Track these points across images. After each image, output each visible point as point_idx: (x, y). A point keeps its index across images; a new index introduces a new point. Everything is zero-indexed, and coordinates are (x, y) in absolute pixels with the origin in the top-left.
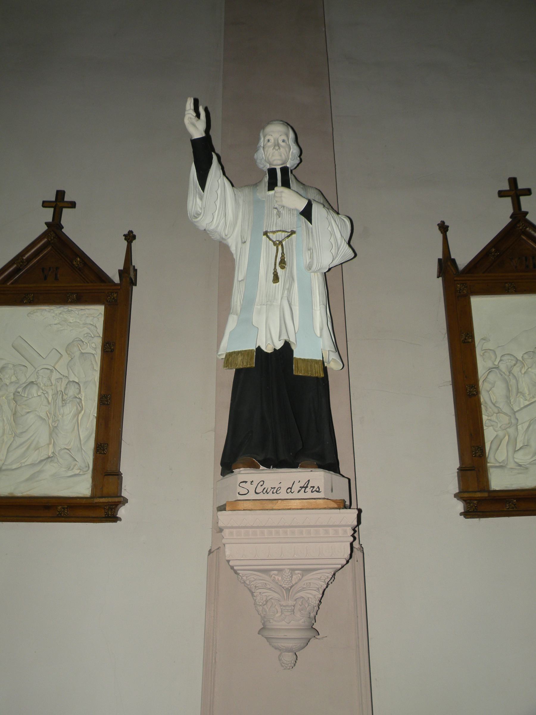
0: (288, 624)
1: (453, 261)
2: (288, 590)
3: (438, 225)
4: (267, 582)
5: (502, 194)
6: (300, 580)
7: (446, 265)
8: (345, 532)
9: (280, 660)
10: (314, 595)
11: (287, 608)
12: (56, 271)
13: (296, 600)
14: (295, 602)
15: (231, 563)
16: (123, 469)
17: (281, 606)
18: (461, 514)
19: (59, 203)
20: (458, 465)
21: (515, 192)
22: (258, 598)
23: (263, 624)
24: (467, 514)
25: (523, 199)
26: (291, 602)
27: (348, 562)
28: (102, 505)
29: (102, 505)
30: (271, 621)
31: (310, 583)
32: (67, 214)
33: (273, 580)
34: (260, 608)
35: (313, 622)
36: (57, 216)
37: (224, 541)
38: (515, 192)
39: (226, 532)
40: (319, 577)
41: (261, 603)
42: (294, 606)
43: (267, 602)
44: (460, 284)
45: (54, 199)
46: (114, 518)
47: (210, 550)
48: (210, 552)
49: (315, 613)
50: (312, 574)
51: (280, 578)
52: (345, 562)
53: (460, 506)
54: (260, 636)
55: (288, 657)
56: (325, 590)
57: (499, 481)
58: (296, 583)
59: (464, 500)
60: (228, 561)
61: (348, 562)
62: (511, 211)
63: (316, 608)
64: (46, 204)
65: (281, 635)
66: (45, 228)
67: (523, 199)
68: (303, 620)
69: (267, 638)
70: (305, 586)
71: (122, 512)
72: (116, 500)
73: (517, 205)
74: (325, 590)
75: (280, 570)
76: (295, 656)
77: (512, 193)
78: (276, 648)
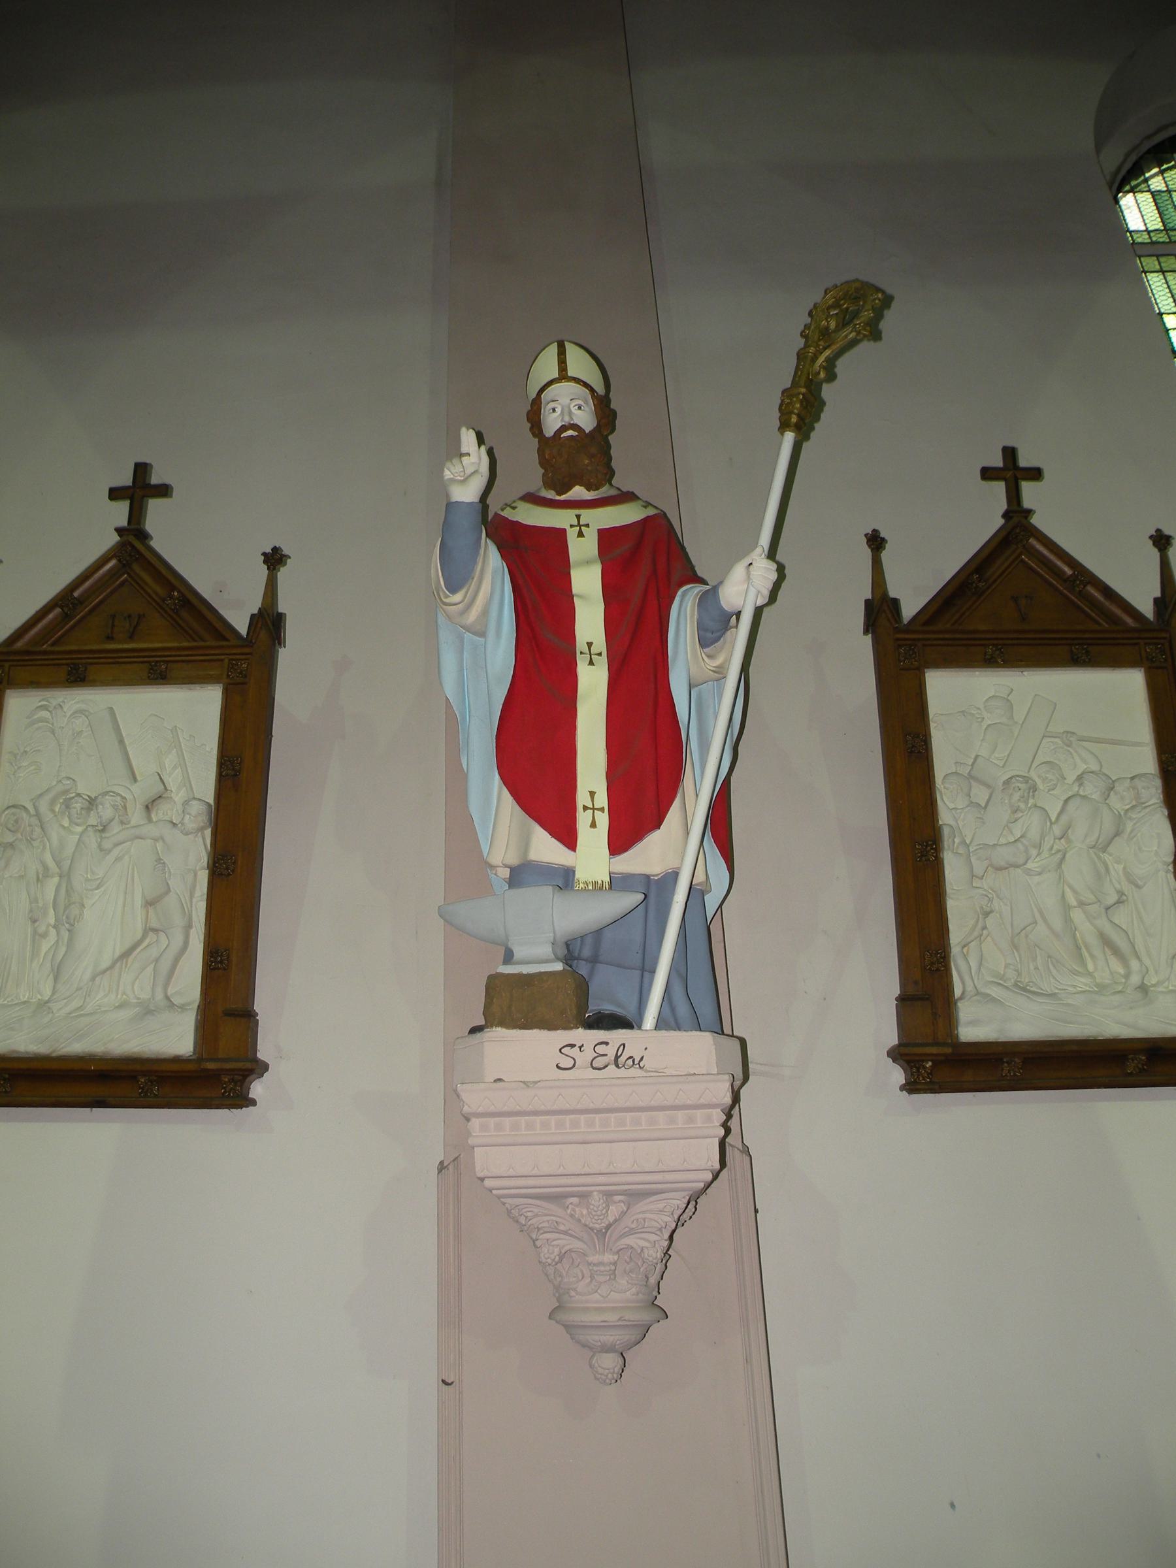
0: (608, 1299)
1: (895, 603)
2: (602, 1233)
3: (866, 535)
4: (558, 1219)
5: (988, 474)
6: (624, 1213)
7: (880, 612)
8: (709, 1119)
9: (591, 1366)
10: (651, 1245)
11: (602, 1268)
12: (130, 619)
13: (618, 1252)
14: (616, 1257)
15: (488, 1183)
16: (258, 1007)
17: (590, 1264)
18: (902, 1088)
19: (140, 489)
20: (897, 992)
21: (1011, 472)
22: (545, 1250)
23: (558, 1300)
24: (911, 1087)
25: (1028, 489)
26: (609, 1257)
27: (716, 1176)
28: (216, 1074)
29: (216, 1074)
30: (572, 1293)
31: (644, 1219)
32: (157, 514)
33: (572, 1216)
34: (551, 1270)
35: (655, 1293)
36: (137, 514)
37: (471, 1141)
38: (1011, 472)
39: (475, 1123)
40: (661, 1206)
41: (549, 1261)
42: (615, 1264)
43: (562, 1256)
44: (909, 645)
45: (129, 483)
46: (241, 1100)
47: (441, 1163)
48: (442, 1167)
49: (659, 1277)
50: (648, 1200)
51: (585, 1212)
52: (710, 1177)
53: (897, 1075)
54: (553, 1322)
55: (610, 1362)
56: (674, 1231)
57: (976, 1024)
58: (616, 1221)
59: (908, 1062)
60: (482, 1179)
61: (716, 1176)
62: (1004, 506)
63: (660, 1267)
64: (115, 494)
65: (596, 1318)
66: (116, 538)
67: (1027, 487)
68: (634, 1290)
69: (567, 1327)
70: (633, 1226)
71: (257, 1089)
72: (248, 1065)
73: (1014, 495)
74: (674, 1231)
75: (584, 1196)
76: (621, 1361)
77: (1009, 474)
78: (584, 1346)
